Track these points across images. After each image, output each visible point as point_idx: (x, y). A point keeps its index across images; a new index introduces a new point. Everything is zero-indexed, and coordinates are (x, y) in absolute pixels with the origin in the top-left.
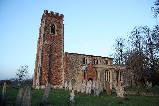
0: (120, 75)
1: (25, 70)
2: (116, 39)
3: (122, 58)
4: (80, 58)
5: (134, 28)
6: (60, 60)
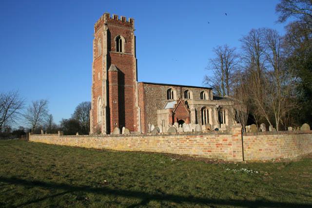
0: (225, 115)
1: (42, 110)
2: (217, 50)
3: (227, 83)
4: (164, 90)
5: (249, 31)
6: (133, 94)
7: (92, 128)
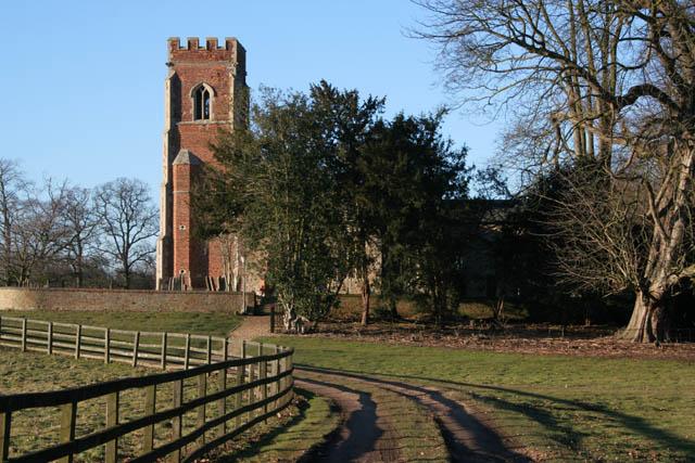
7: (161, 281)
